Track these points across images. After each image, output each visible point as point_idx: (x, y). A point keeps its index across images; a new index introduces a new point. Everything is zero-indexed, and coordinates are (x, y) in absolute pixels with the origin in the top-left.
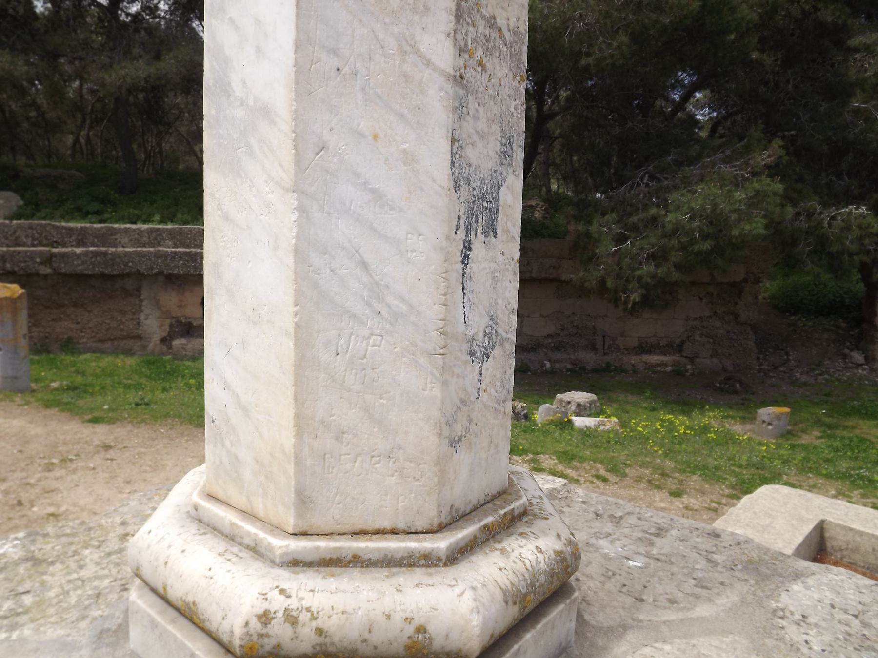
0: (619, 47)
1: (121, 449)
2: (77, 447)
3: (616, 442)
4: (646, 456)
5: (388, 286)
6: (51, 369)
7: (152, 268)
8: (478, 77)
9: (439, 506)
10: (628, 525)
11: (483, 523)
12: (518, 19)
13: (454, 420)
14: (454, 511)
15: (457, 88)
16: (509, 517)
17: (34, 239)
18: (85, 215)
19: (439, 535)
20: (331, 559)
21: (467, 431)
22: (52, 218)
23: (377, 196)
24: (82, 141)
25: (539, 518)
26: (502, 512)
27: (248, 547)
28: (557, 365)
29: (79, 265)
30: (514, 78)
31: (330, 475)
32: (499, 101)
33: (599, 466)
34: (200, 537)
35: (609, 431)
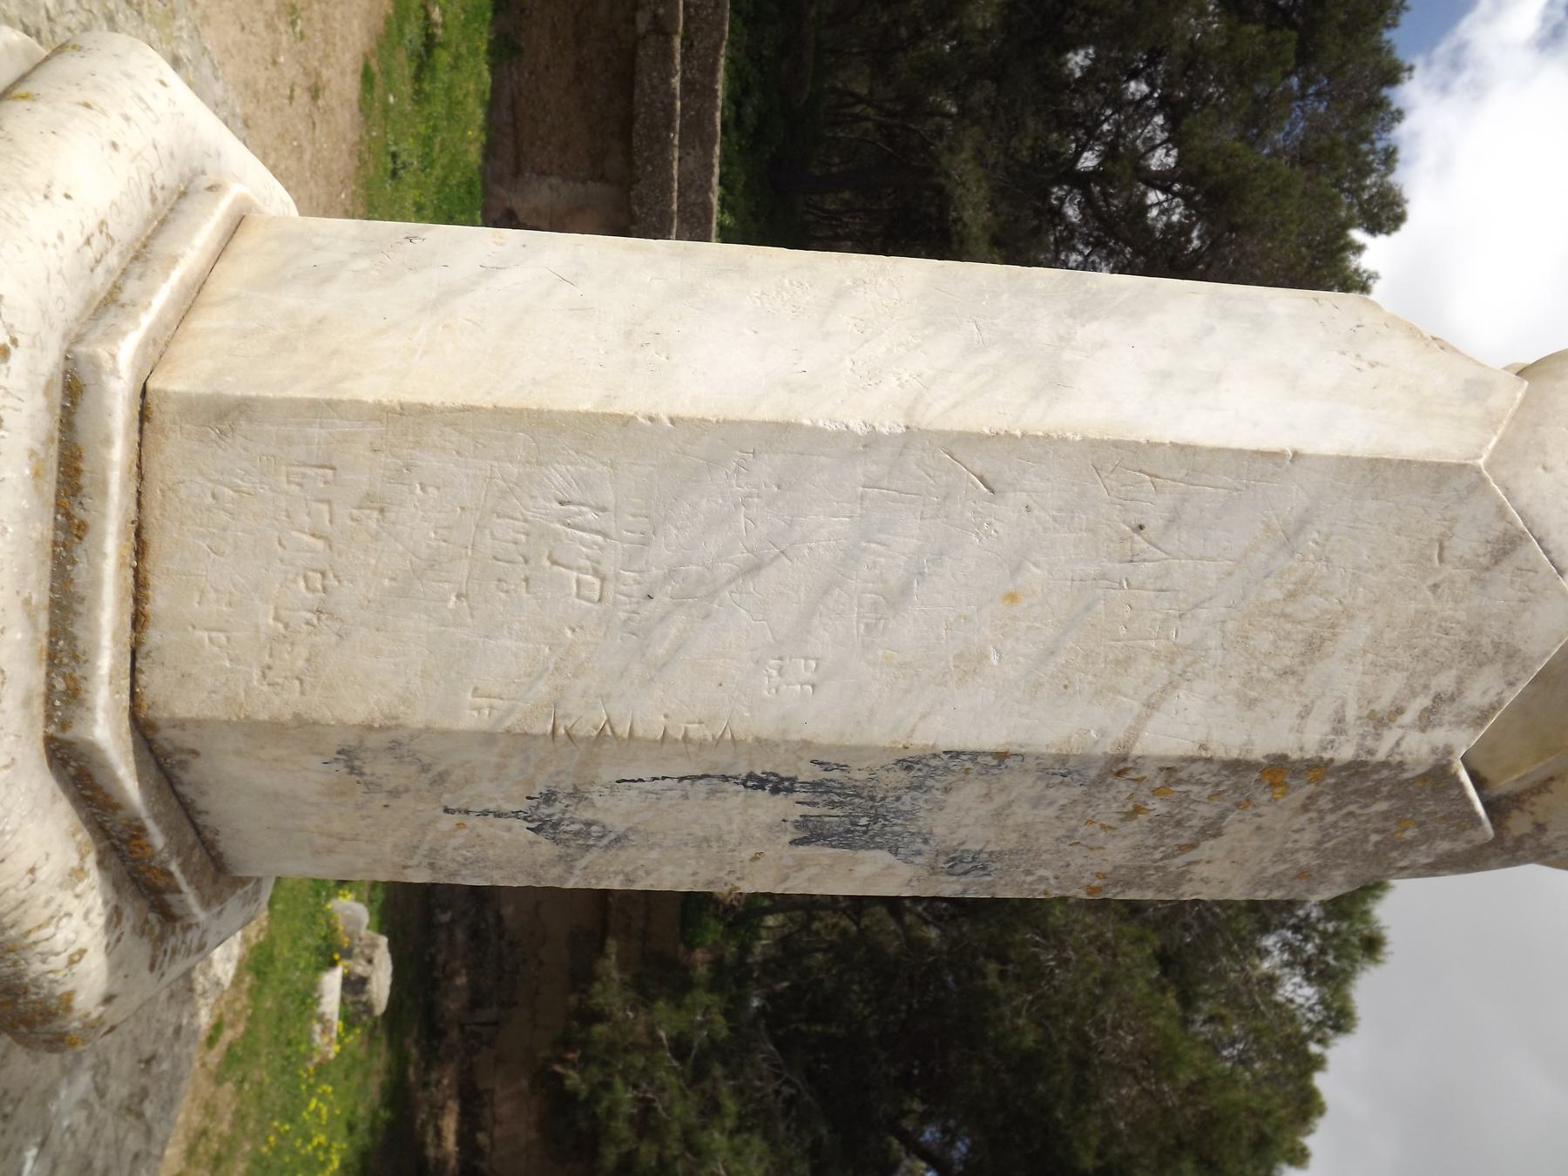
0: (1016, 1029)
1: (310, 116)
2: (318, 39)
3: (288, 1058)
4: (259, 1122)
5: (707, 616)
6: (464, 10)
7: (641, 205)
8: (1115, 805)
9: (199, 723)
10: (121, 1134)
11: (151, 825)
12: (1205, 881)
13: (400, 759)
14: (184, 757)
15: (1102, 763)
16: (161, 882)
17: (697, 8)
18: (736, 100)
19: (126, 724)
20: (78, 471)
21: (372, 787)
22: (731, 43)
23: (895, 599)
24: (858, 109)
25: (155, 948)
26: (174, 867)
27: (117, 288)
28: (443, 936)
29: (650, 80)
30: (1097, 875)
31: (284, 479)
32: (1062, 846)
33: (241, 1028)
34: (146, 188)
35: (310, 1040)
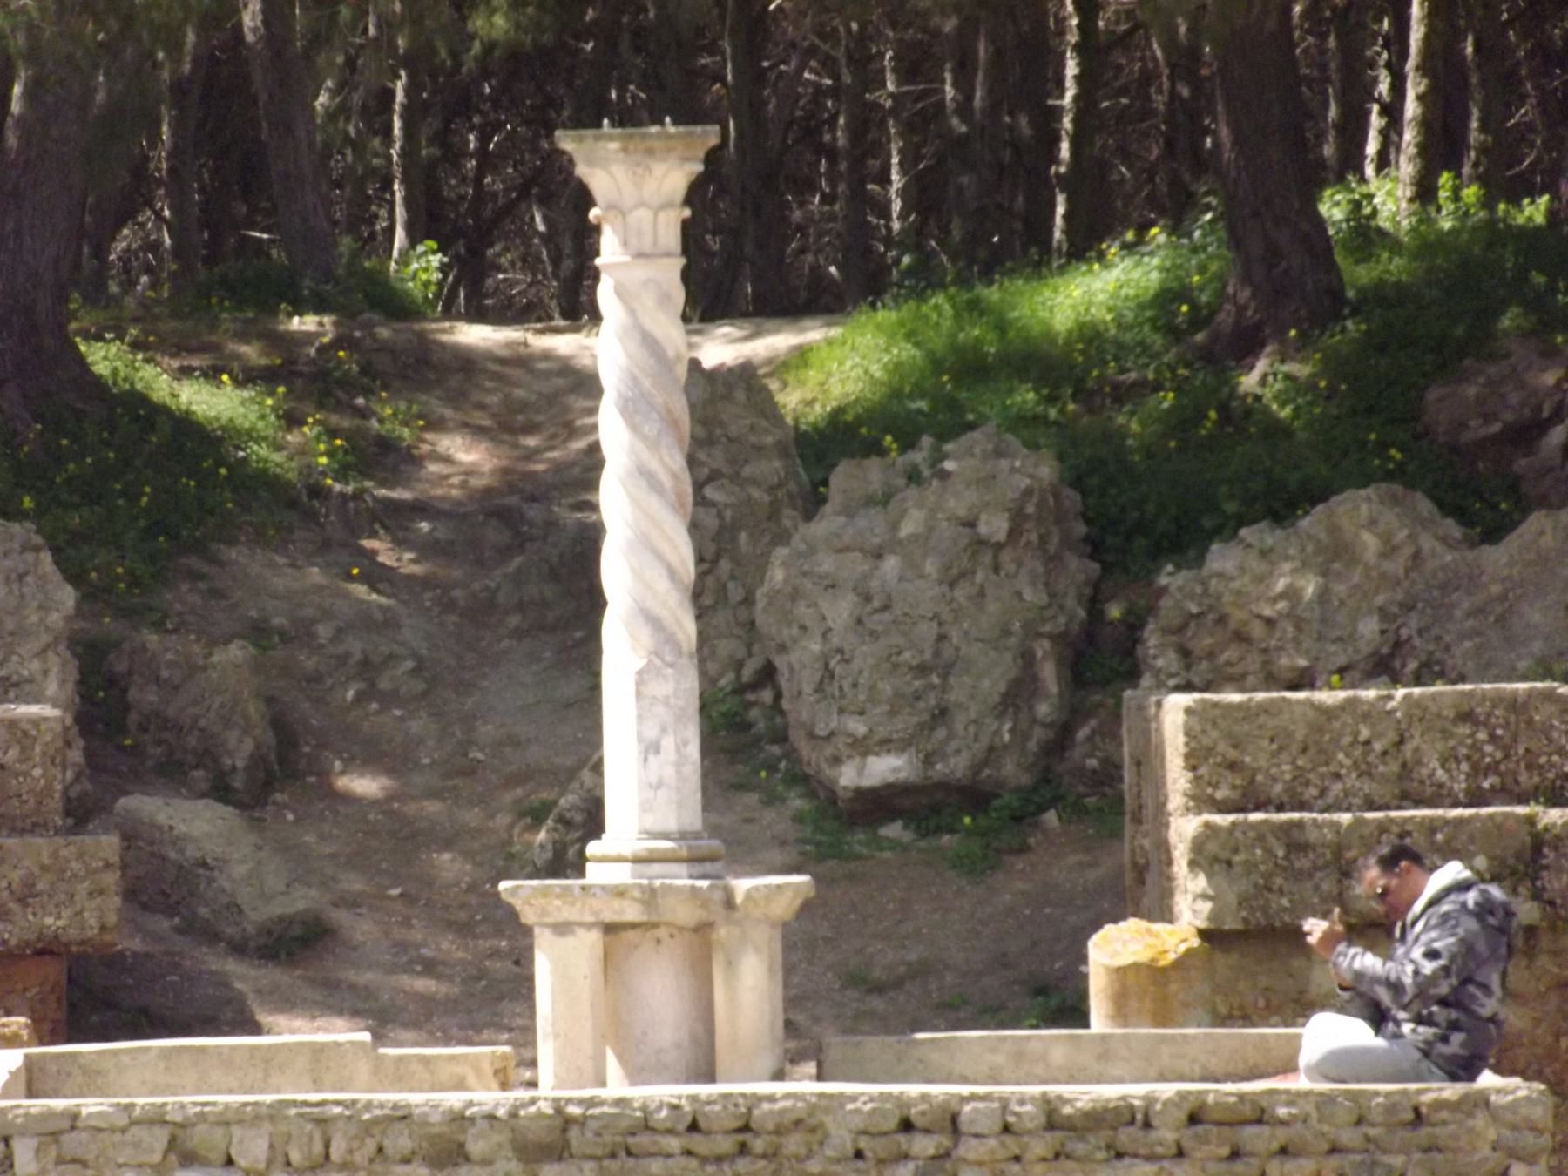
16: (1348, 677)
17: (1477, 771)
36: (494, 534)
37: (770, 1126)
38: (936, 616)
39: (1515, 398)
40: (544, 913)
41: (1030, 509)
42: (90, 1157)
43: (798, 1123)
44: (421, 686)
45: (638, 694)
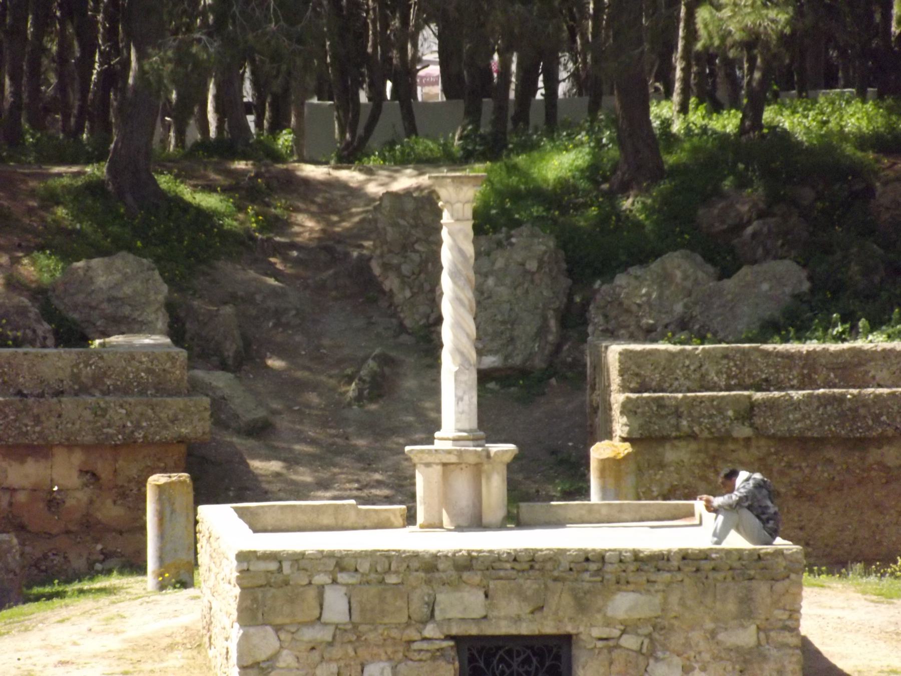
17: (729, 377)
29: (798, 421)
36: (323, 257)
37: (541, 559)
38: (509, 301)
39: (733, 214)
40: (421, 459)
41: (546, 259)
42: (309, 568)
43: (550, 559)
44: (298, 321)
45: (456, 380)
